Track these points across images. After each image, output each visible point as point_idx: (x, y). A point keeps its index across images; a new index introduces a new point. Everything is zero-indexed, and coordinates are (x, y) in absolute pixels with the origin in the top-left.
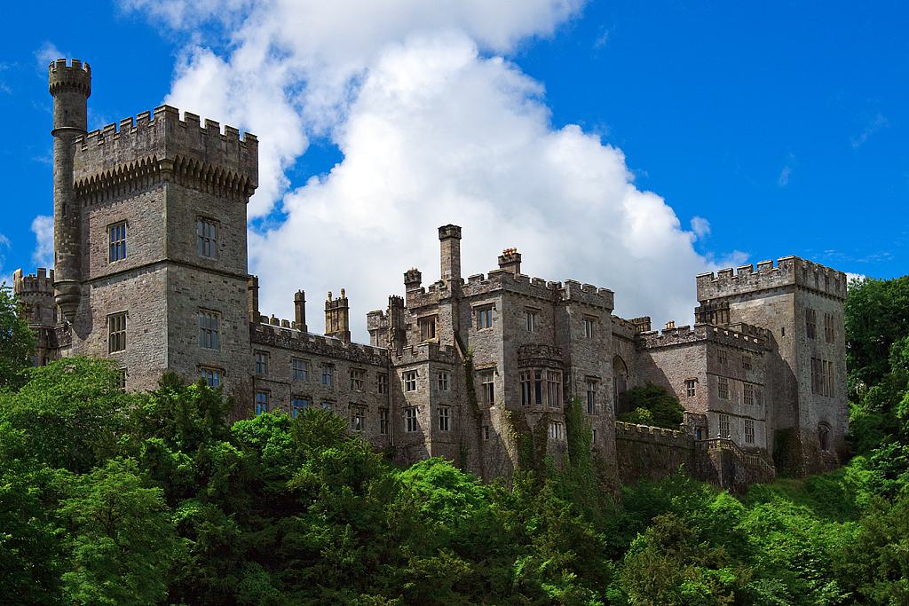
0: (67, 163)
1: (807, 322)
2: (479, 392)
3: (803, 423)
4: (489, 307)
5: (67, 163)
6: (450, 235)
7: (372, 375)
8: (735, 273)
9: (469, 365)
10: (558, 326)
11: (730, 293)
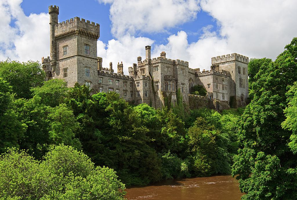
0: (53, 31)
2: (155, 87)
4: (157, 66)
7: (129, 83)
8: (221, 57)
10: (175, 71)
11: (219, 62)
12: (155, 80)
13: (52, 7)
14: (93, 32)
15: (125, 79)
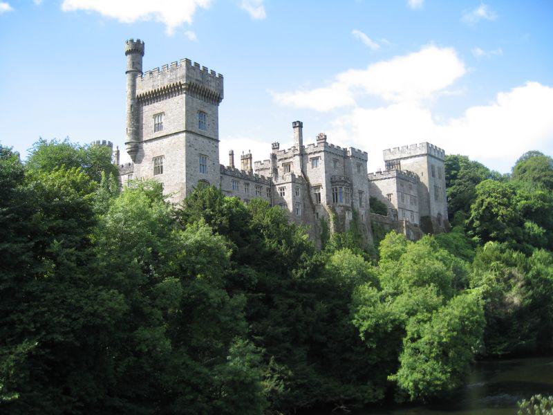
0: (134, 86)
1: (432, 171)
2: (314, 197)
3: (432, 214)
4: (317, 158)
5: (134, 86)
7: (265, 187)
8: (400, 149)
9: (308, 184)
12: (313, 182)
13: (132, 41)
14: (212, 88)
15: (259, 181)
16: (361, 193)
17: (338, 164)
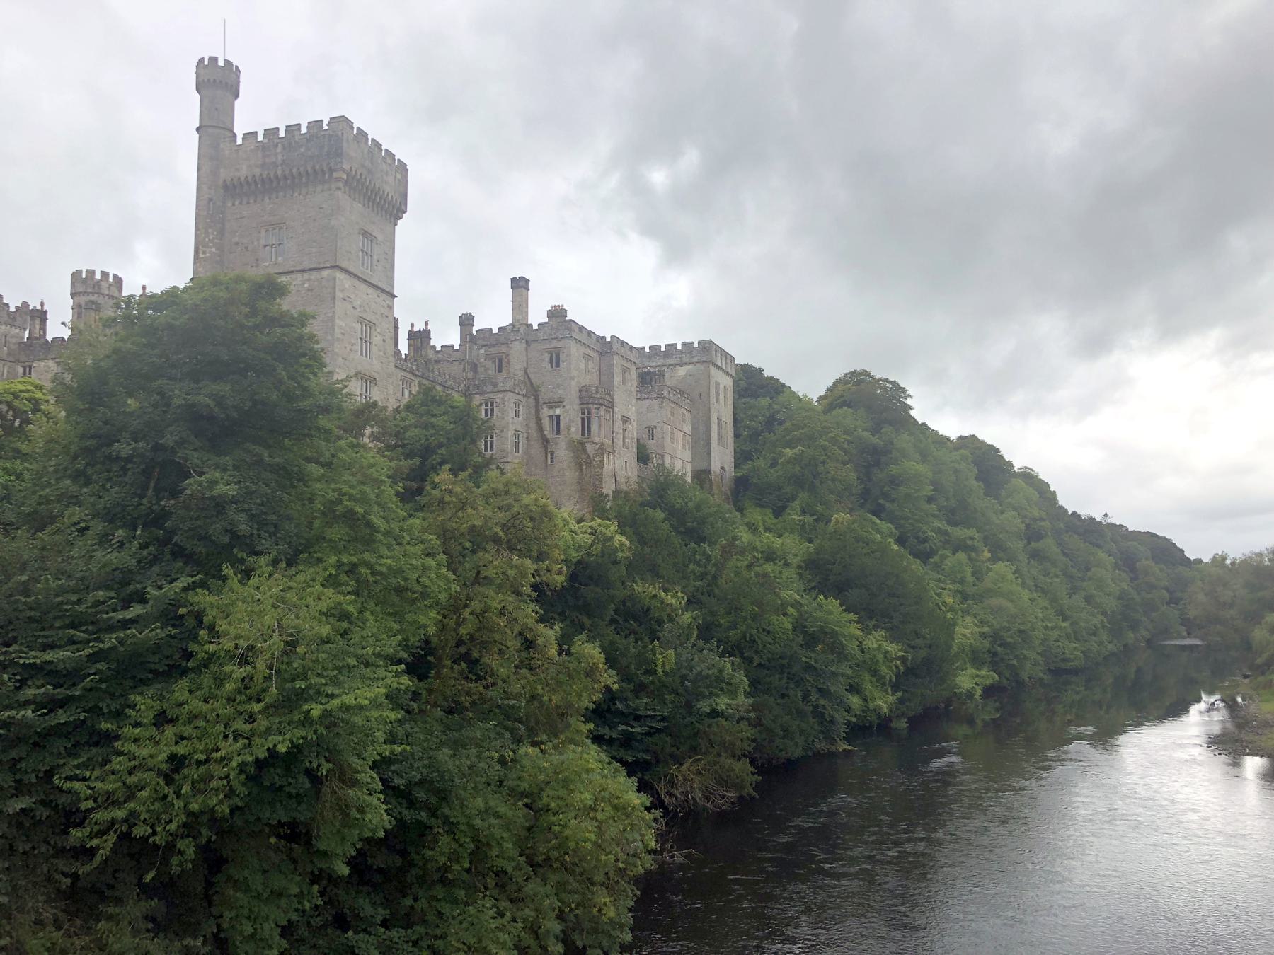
6: (520, 285)
10: (606, 374)
11: (659, 364)
14: (389, 189)
16: (625, 420)
17: (591, 365)
